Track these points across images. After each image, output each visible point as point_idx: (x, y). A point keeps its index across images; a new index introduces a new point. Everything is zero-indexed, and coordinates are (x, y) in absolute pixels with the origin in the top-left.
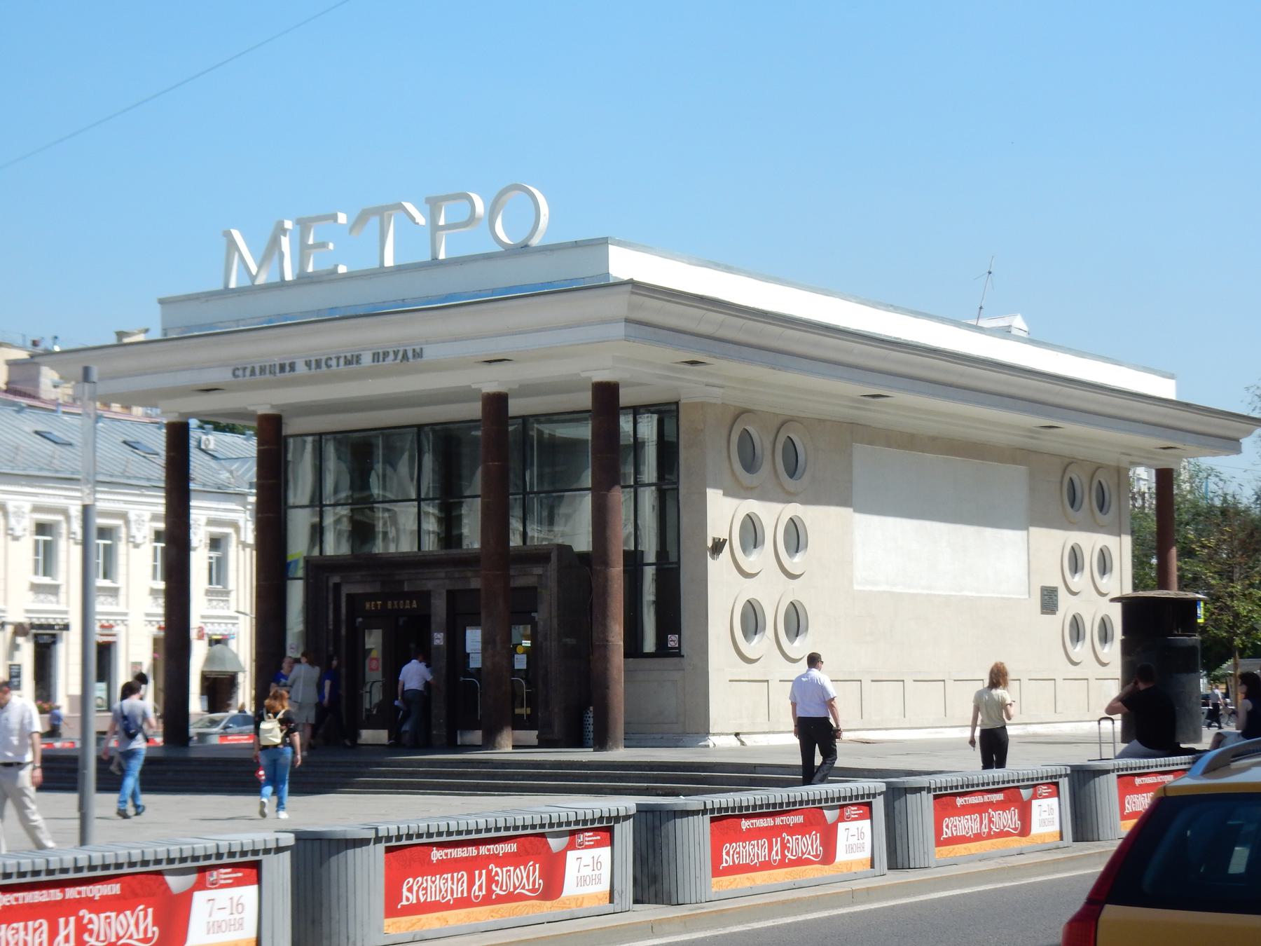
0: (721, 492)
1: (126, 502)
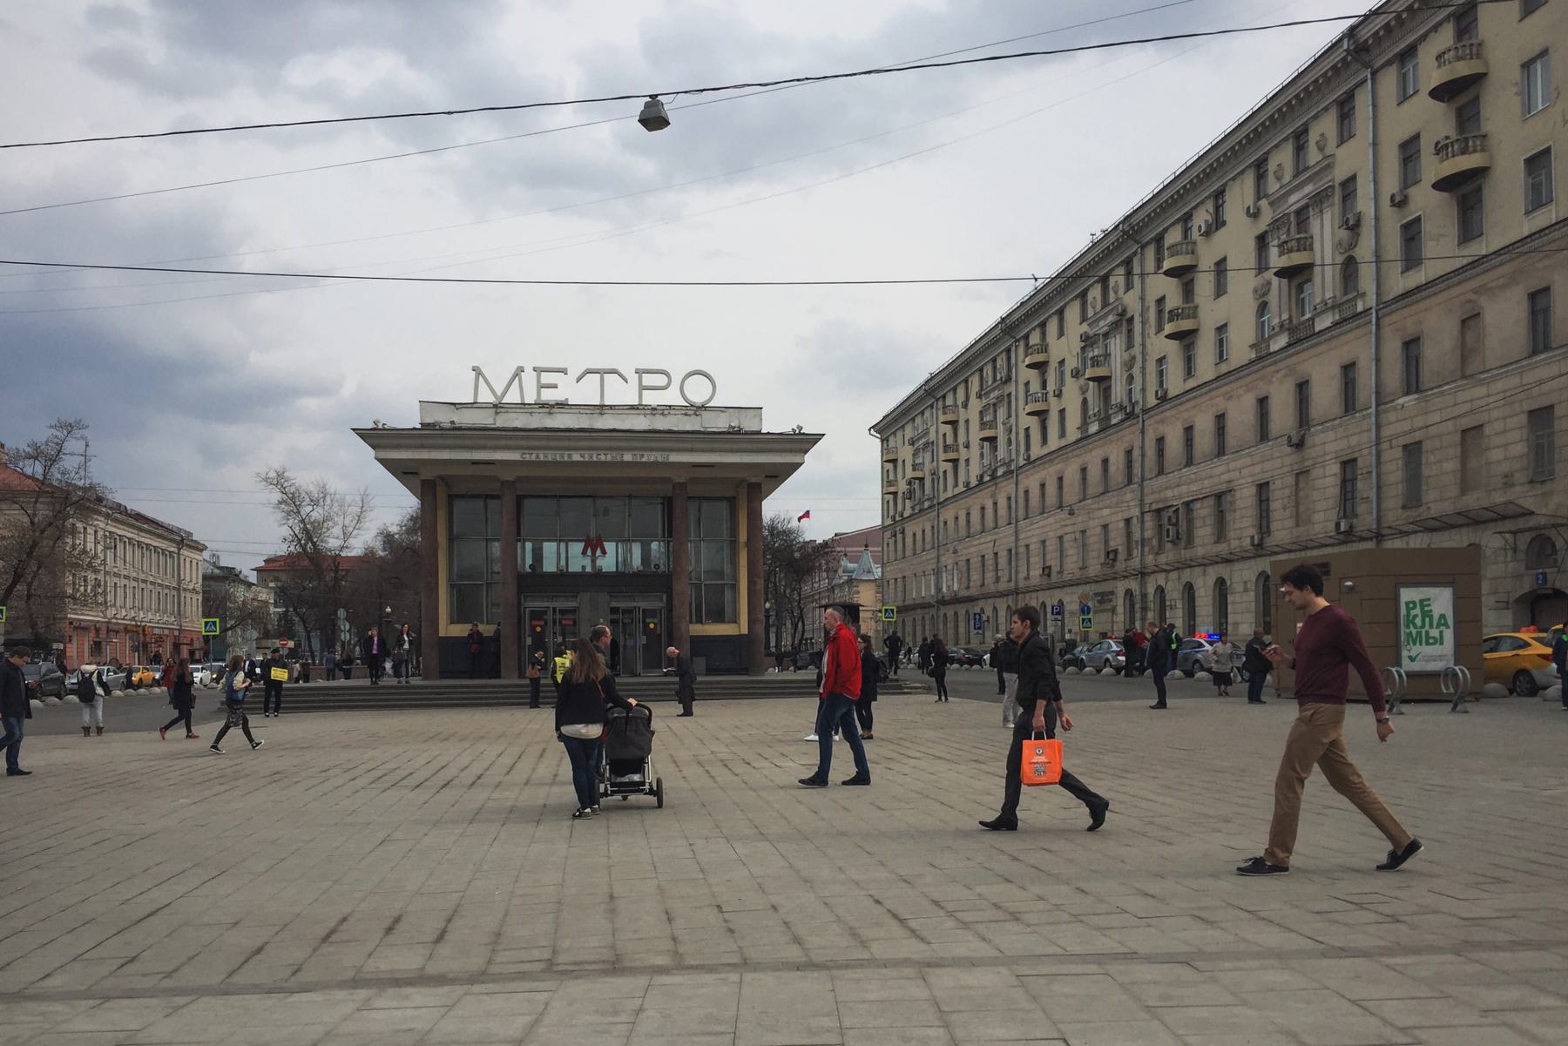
0: (1268, 846)
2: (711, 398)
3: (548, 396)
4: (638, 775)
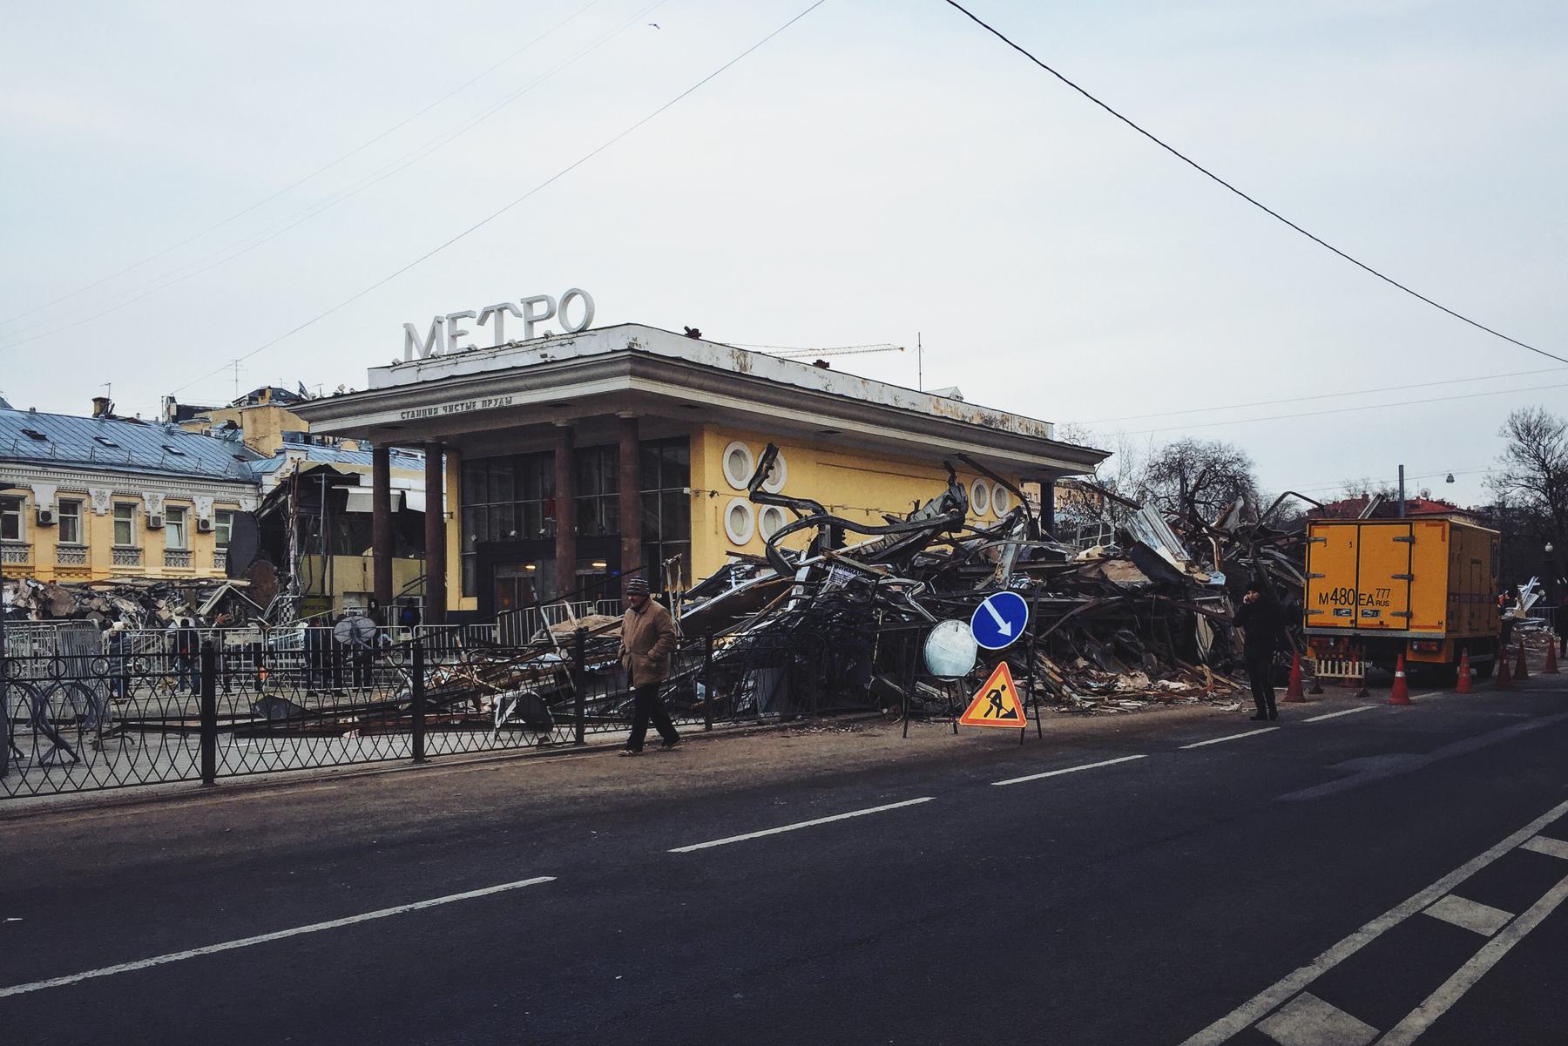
1: (30, 478)
2: (588, 320)
3: (462, 344)
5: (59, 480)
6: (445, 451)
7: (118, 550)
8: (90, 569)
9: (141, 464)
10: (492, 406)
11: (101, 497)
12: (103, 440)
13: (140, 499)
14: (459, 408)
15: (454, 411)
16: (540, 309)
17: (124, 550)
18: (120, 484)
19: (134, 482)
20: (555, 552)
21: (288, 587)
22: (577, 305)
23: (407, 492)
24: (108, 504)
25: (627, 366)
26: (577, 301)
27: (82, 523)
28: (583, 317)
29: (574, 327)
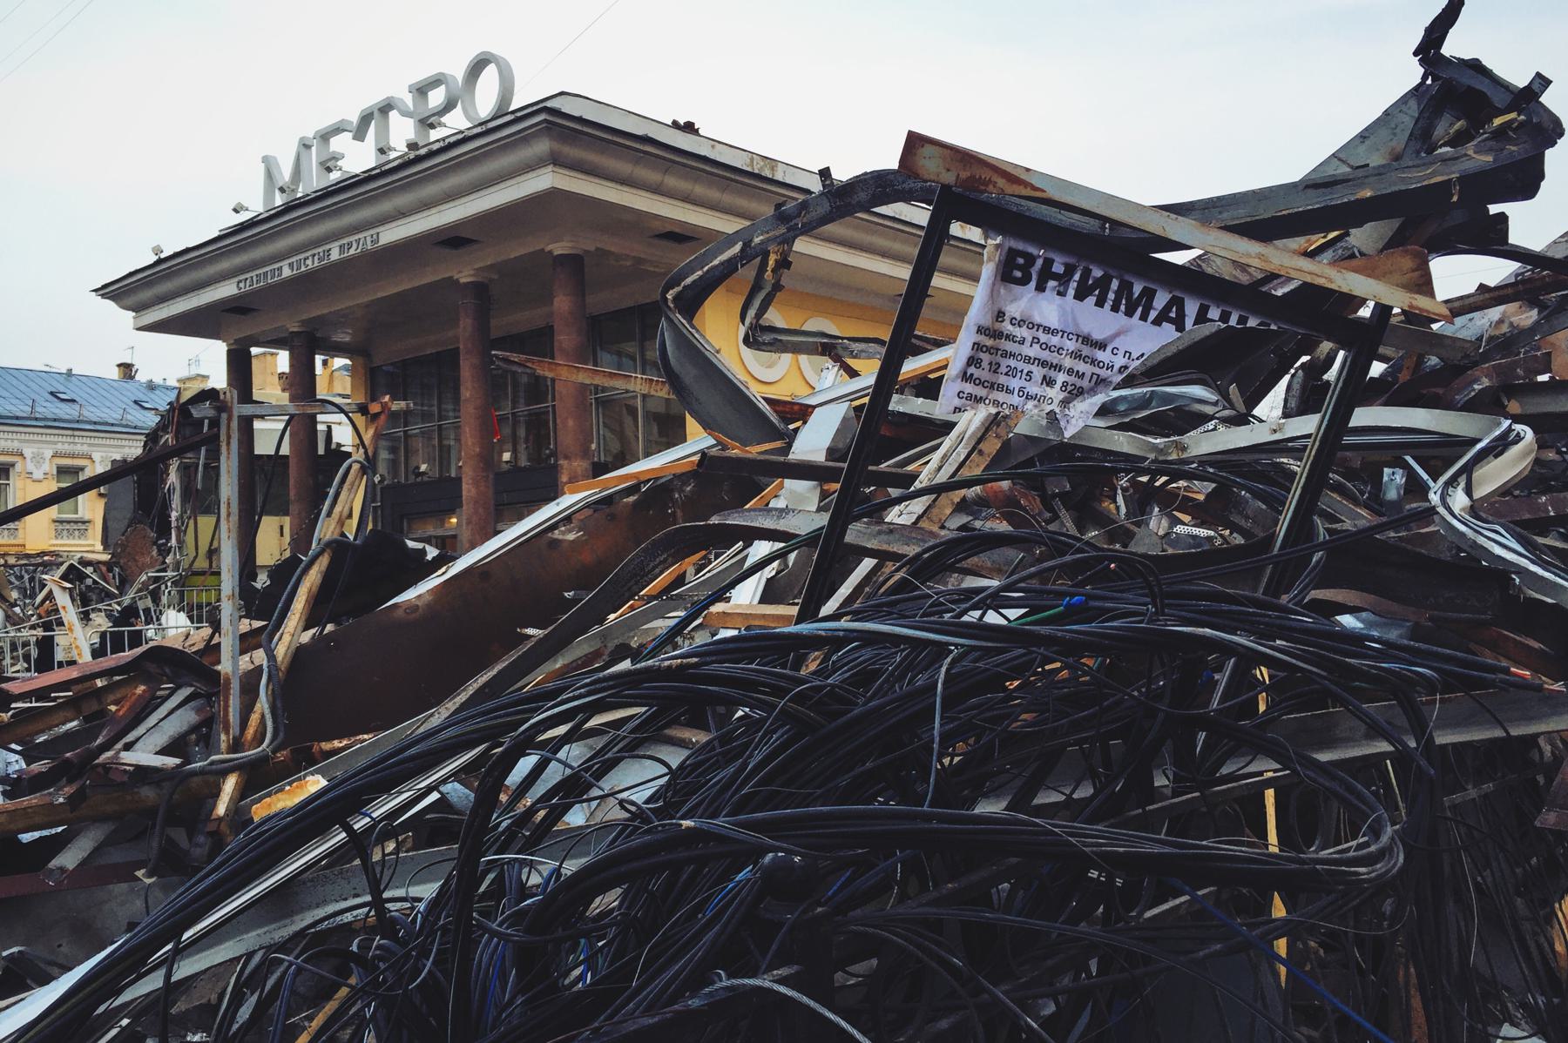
0: (1174, 327)
4: (723, 708)
5: (56, 443)
6: (360, 360)
7: (61, 522)
8: (24, 546)
9: (67, 417)
10: (352, 251)
11: (39, 459)
12: (58, 395)
13: (90, 460)
14: (309, 262)
15: (303, 269)
16: (436, 98)
17: (69, 522)
18: (130, 447)
19: (80, 440)
20: (462, 497)
21: (167, 561)
22: (489, 82)
23: (333, 425)
24: (49, 467)
25: (542, 146)
26: (490, 75)
27: (15, 492)
28: (495, 101)
29: (483, 117)
